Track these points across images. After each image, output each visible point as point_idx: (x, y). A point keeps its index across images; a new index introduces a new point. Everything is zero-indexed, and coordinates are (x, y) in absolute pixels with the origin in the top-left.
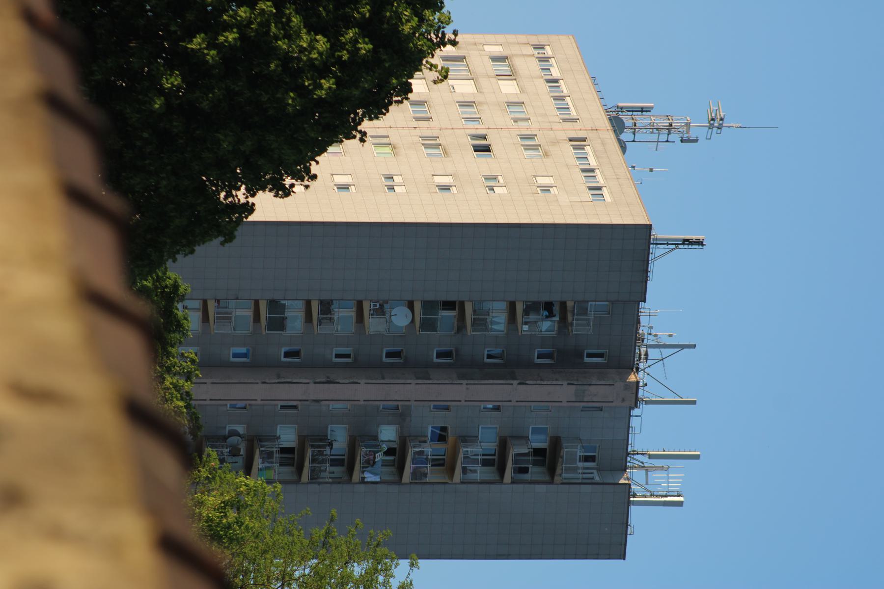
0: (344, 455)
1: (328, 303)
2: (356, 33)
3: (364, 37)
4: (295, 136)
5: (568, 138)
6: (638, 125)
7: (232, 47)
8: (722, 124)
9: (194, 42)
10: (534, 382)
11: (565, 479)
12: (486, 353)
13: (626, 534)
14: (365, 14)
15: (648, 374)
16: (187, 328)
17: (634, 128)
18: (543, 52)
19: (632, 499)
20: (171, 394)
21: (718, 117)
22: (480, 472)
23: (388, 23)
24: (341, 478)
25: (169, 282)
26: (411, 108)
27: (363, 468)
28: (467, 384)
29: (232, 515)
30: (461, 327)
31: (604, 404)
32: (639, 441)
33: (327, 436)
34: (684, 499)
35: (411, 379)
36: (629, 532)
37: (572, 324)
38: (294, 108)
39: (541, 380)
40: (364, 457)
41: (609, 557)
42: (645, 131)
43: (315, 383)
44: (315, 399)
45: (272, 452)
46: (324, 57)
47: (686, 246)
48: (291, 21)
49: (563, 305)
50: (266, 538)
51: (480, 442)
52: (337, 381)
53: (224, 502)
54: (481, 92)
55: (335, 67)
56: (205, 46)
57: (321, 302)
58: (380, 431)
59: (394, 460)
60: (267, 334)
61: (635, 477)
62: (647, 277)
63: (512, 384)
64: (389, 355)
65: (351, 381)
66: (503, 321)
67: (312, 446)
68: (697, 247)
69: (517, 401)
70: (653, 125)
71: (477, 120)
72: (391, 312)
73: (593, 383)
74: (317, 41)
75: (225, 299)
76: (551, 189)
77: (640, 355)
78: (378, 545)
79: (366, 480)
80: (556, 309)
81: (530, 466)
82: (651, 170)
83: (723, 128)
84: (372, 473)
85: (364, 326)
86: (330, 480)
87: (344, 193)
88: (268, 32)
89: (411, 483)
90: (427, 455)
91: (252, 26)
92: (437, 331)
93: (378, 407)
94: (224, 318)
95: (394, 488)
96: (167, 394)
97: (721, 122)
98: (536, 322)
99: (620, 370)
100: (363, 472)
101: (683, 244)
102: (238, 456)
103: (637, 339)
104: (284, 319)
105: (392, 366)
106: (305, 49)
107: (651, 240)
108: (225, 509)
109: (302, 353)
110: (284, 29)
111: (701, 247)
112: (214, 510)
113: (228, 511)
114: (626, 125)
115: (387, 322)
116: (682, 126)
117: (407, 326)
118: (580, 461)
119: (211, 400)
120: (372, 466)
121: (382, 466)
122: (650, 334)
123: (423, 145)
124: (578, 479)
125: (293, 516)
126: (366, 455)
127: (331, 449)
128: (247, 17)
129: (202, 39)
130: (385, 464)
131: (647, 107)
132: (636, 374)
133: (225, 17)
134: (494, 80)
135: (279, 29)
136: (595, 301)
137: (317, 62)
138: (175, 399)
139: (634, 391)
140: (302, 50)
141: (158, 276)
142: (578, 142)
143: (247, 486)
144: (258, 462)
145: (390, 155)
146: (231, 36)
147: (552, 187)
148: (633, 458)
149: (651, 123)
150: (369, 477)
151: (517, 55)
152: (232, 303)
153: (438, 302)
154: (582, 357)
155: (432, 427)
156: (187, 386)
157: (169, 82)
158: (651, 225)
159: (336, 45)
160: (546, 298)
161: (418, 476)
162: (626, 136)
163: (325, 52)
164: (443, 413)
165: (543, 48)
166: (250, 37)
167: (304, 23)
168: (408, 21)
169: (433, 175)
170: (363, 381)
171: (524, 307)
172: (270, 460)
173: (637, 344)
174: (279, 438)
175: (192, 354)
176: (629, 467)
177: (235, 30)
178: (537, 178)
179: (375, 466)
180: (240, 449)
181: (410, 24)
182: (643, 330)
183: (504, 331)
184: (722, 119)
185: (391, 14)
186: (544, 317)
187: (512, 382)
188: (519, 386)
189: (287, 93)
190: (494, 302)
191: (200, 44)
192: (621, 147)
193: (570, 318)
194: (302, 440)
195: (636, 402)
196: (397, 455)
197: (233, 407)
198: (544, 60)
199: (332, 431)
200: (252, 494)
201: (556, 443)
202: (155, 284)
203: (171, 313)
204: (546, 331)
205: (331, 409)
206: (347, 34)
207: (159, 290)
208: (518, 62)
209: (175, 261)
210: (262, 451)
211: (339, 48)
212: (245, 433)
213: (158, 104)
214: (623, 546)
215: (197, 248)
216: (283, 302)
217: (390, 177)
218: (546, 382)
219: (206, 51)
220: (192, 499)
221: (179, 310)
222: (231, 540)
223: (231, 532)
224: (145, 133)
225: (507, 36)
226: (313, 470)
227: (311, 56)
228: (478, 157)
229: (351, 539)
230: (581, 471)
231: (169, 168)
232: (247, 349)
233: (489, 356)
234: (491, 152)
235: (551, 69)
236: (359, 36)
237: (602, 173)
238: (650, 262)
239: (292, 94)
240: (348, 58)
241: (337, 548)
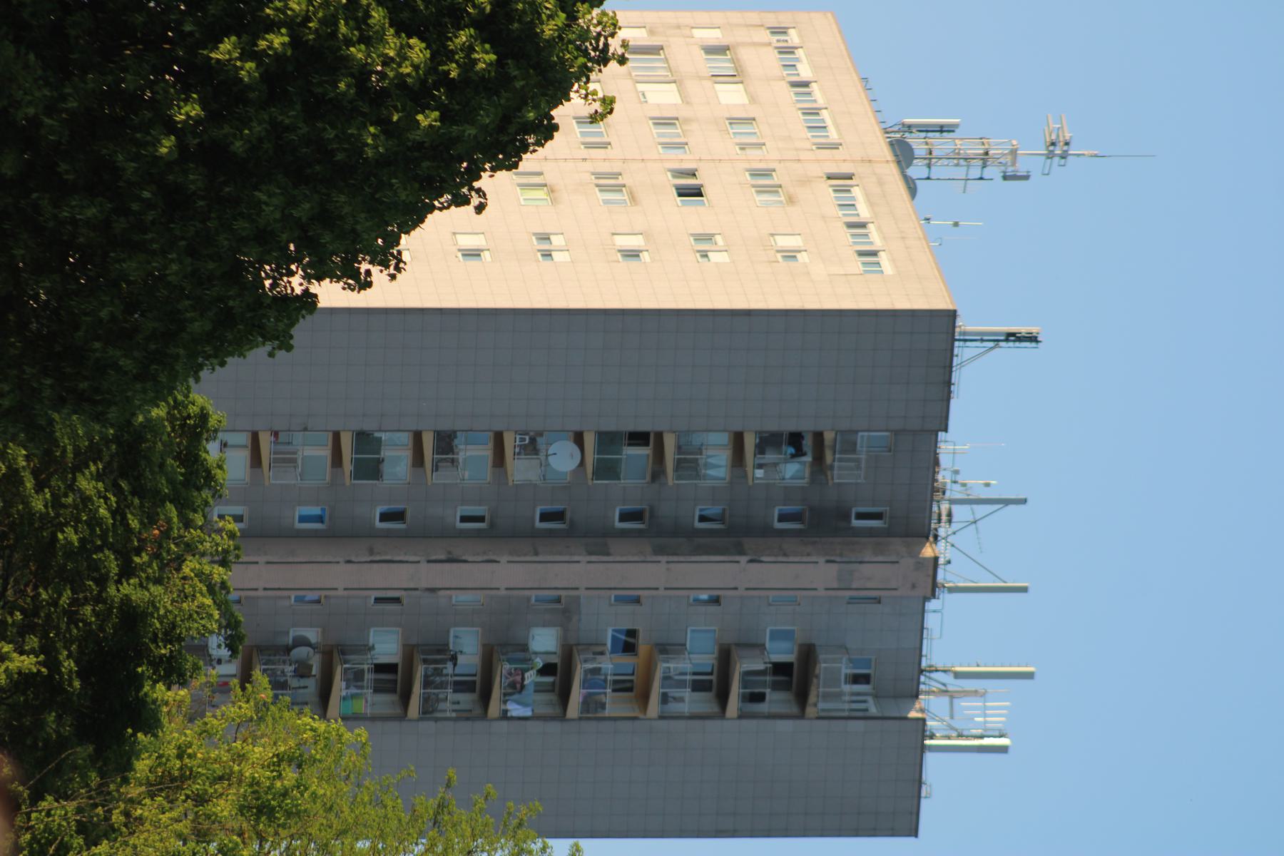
0: (475, 675)
1: (449, 436)
2: (471, 36)
3: (483, 42)
4: (377, 196)
5: (826, 174)
6: (935, 153)
7: (279, 58)
8: (1066, 151)
9: (221, 49)
11: (823, 710)
13: (919, 797)
14: (485, 8)
15: (953, 545)
16: (221, 481)
17: (929, 159)
19: (928, 742)
20: (193, 587)
21: (1061, 139)
22: (690, 701)
23: (520, 21)
24: (470, 711)
25: (193, 410)
26: (579, 128)
27: (505, 695)
28: (668, 562)
29: (290, 775)
30: (658, 473)
32: (936, 651)
33: (447, 645)
34: (1012, 741)
35: (579, 555)
36: (923, 794)
37: (832, 467)
38: (375, 151)
39: (785, 555)
40: (507, 678)
41: (893, 832)
42: (945, 161)
43: (429, 561)
44: (429, 586)
45: (363, 671)
46: (421, 72)
47: (1011, 344)
48: (370, 17)
49: (818, 437)
50: (342, 812)
51: (689, 654)
52: (464, 558)
53: (278, 755)
54: (688, 103)
55: (438, 90)
56: (237, 55)
57: (438, 435)
58: (531, 635)
59: (554, 683)
60: (354, 484)
62: (950, 392)
63: (738, 562)
64: (545, 517)
65: (485, 558)
66: (723, 463)
67: (425, 661)
68: (1027, 344)
69: (747, 589)
70: (959, 154)
72: (547, 450)
73: (866, 560)
74: (410, 47)
75: (286, 431)
76: (798, 255)
77: (940, 515)
78: (520, 825)
79: (509, 714)
80: (808, 443)
81: (768, 691)
82: (956, 224)
83: (1070, 158)
84: (519, 703)
85: (506, 473)
86: (454, 715)
87: (473, 263)
88: (334, 34)
89: (580, 719)
90: (606, 675)
91: (311, 25)
92: (619, 479)
93: (529, 599)
94: (284, 461)
95: (554, 727)
96: (186, 586)
97: (1066, 148)
98: (775, 465)
99: (909, 539)
100: (505, 702)
101: (1007, 340)
102: (309, 677)
103: (933, 490)
104: (380, 461)
105: (550, 534)
106: (392, 59)
107: (956, 334)
108: (279, 766)
109: (408, 515)
110: (359, 29)
111: (1034, 344)
112: (263, 768)
113: (284, 769)
114: (917, 153)
115: (541, 465)
117: (574, 472)
118: (846, 683)
119: (265, 589)
120: (520, 692)
121: (535, 691)
122: (955, 482)
123: (597, 186)
125: (387, 778)
126: (510, 674)
127: (455, 665)
128: (301, 10)
129: (234, 44)
130: (539, 689)
132: (934, 545)
133: (268, 11)
134: (708, 84)
135: (352, 30)
136: (868, 431)
137: (409, 80)
138: (198, 595)
139: (931, 572)
140: (387, 61)
141: (175, 400)
142: (841, 180)
143: (315, 731)
144: (339, 687)
146: (278, 40)
147: (800, 251)
148: (930, 678)
149: (955, 149)
150: (515, 709)
151: (744, 44)
152: (298, 437)
154: (846, 517)
155: (614, 630)
156: (218, 573)
157: (183, 111)
158: (955, 311)
159: (440, 53)
160: (791, 426)
161: (592, 707)
162: (916, 170)
163: (422, 65)
164: (630, 608)
165: (785, 33)
166: (307, 41)
167: (390, 19)
168: (550, 17)
169: (613, 234)
170: (504, 559)
171: (758, 440)
172: (359, 684)
173: (935, 498)
174: (373, 648)
175: (230, 523)
176: (922, 691)
177: (283, 31)
178: (776, 237)
179: (523, 692)
180: (312, 666)
181: (554, 23)
182: (943, 477)
183: (725, 479)
184: (1067, 144)
185: (524, 7)
186: (789, 457)
187: (737, 558)
189: (365, 127)
190: (710, 434)
191: (229, 52)
192: (909, 188)
193: (829, 457)
194: (409, 652)
195: (934, 589)
196: (558, 675)
197: (300, 600)
198: (787, 51)
199: (456, 637)
200: (321, 744)
201: (808, 654)
202: (172, 412)
203: (197, 457)
204: (792, 478)
205: (454, 602)
206: (456, 37)
207: (178, 423)
208: (746, 55)
209: (197, 380)
210: (346, 670)
211: (444, 59)
212: (319, 641)
213: (166, 147)
214: (914, 817)
215: (229, 360)
216: (377, 435)
219: (238, 64)
220: (228, 751)
221: (211, 452)
222: (289, 814)
223: (289, 801)
224: (145, 192)
225: (729, 14)
226: (426, 700)
227: (401, 70)
228: (683, 205)
229: (479, 816)
230: (847, 698)
231: (183, 243)
232: (322, 509)
233: (703, 519)
234: (702, 196)
235: (799, 66)
236: (476, 41)
237: (879, 229)
238: (954, 369)
239: (372, 129)
240: (459, 75)
241: (454, 825)
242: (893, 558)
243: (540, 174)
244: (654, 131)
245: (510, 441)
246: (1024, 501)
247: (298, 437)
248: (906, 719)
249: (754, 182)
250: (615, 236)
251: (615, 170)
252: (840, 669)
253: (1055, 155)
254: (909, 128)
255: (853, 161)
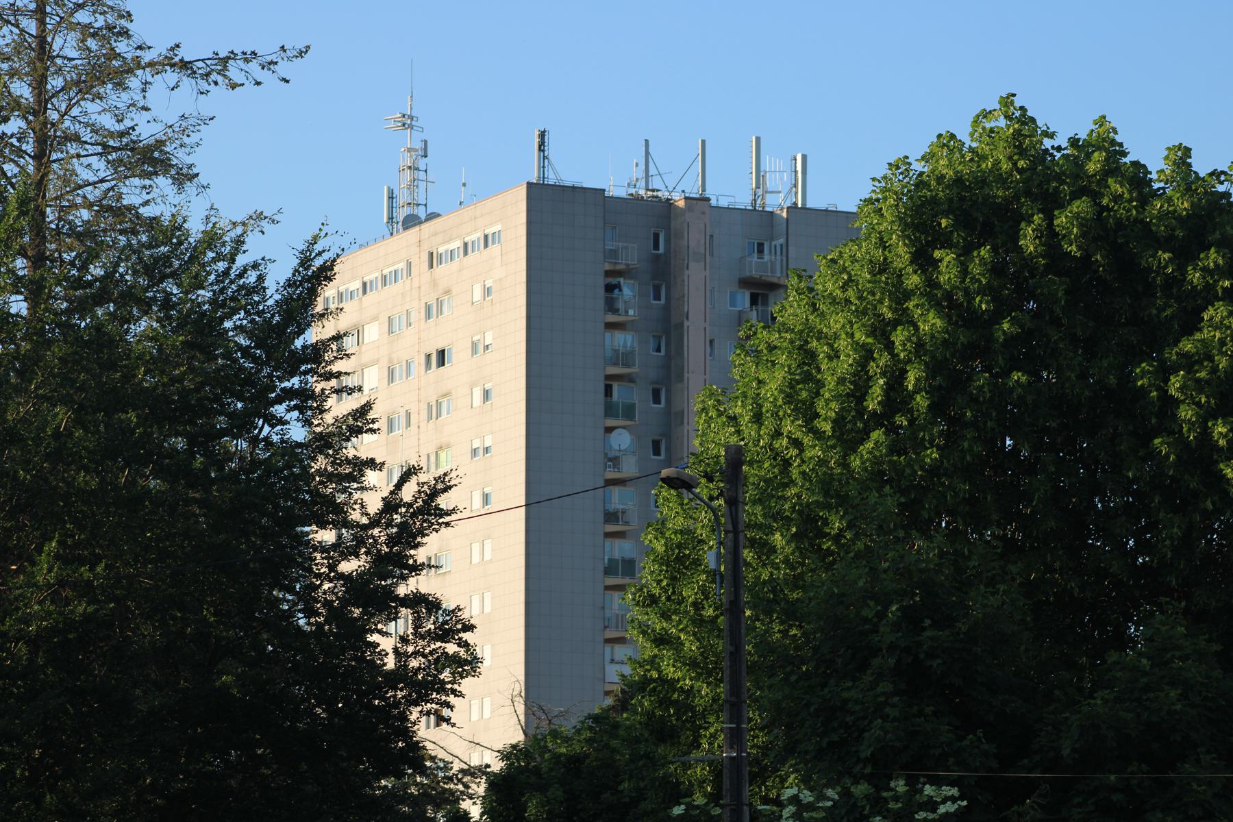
10: (686, 303)
11: (782, 273)
12: (656, 354)
18: (331, 298)
19: (800, 206)
31: (708, 234)
32: (743, 199)
37: (627, 265)
39: (683, 296)
47: (546, 148)
49: (608, 274)
61: (777, 202)
66: (623, 336)
68: (546, 137)
70: (410, 185)
71: (408, 364)
76: (487, 286)
80: (613, 281)
82: (464, 185)
83: (413, 114)
88: (1208, 382)
97: (406, 117)
99: (672, 216)
101: (543, 151)
103: (637, 199)
104: (623, 560)
111: (546, 133)
116: (411, 156)
117: (631, 433)
118: (763, 258)
122: (635, 185)
123: (437, 419)
124: (782, 260)
131: (389, 193)
139: (695, 202)
142: (433, 260)
145: (449, 453)
152: (608, 614)
153: (606, 403)
154: (658, 256)
184: (404, 116)
187: (686, 327)
188: (690, 318)
193: (619, 267)
201: (745, 283)
214: (849, 215)
216: (606, 561)
217: (474, 452)
218: (686, 292)
230: (773, 257)
233: (658, 350)
234: (444, 350)
235: (351, 289)
237: (469, 234)
242: (686, 225)
243: (428, 456)
244: (398, 382)
245: (611, 475)
246: (647, 141)
247: (608, 614)
248: (787, 219)
249: (435, 316)
250: (474, 406)
251: (426, 407)
252: (756, 262)
253: (411, 123)
254: (391, 218)
255: (420, 252)
